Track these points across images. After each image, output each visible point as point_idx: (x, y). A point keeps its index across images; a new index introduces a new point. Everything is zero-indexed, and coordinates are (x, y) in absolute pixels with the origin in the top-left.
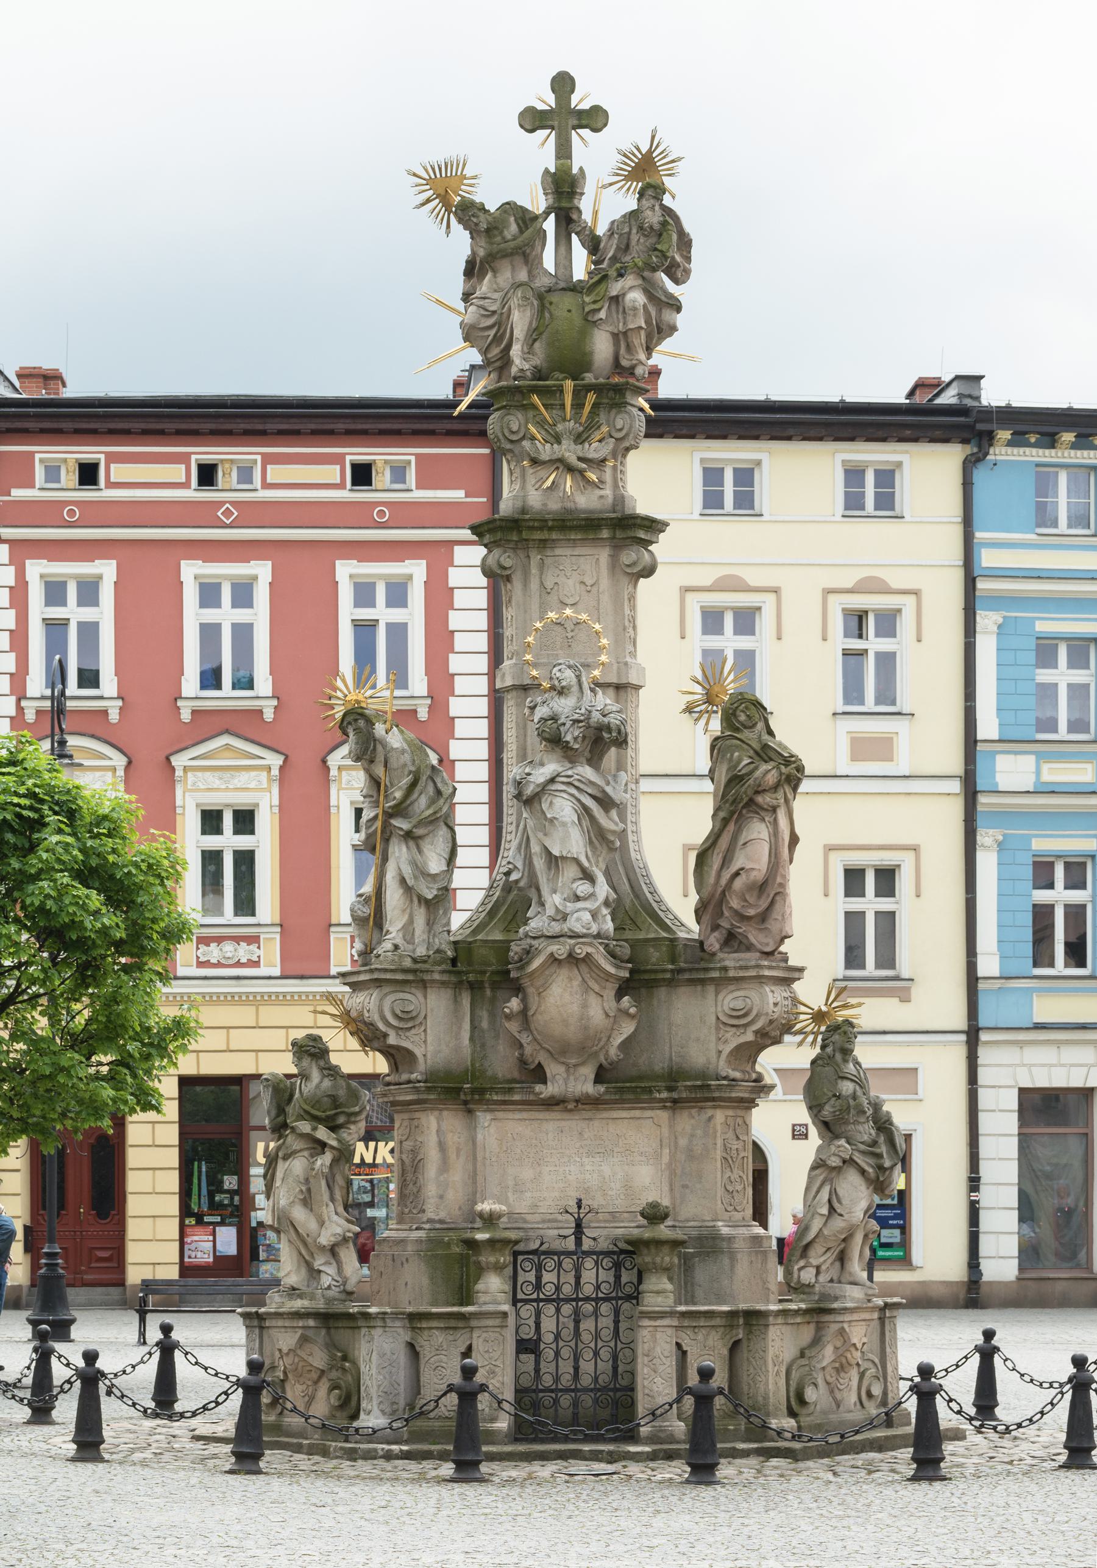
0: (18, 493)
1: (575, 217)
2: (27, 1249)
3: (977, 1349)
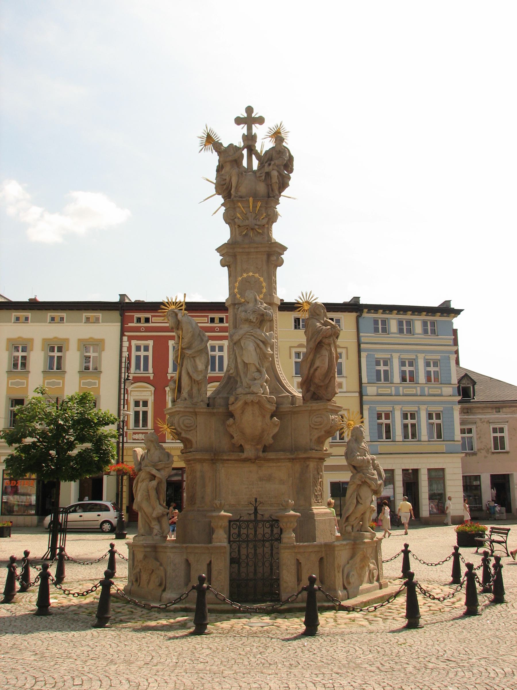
0: (130, 325)
1: (253, 148)
2: (127, 512)
3: (402, 551)
